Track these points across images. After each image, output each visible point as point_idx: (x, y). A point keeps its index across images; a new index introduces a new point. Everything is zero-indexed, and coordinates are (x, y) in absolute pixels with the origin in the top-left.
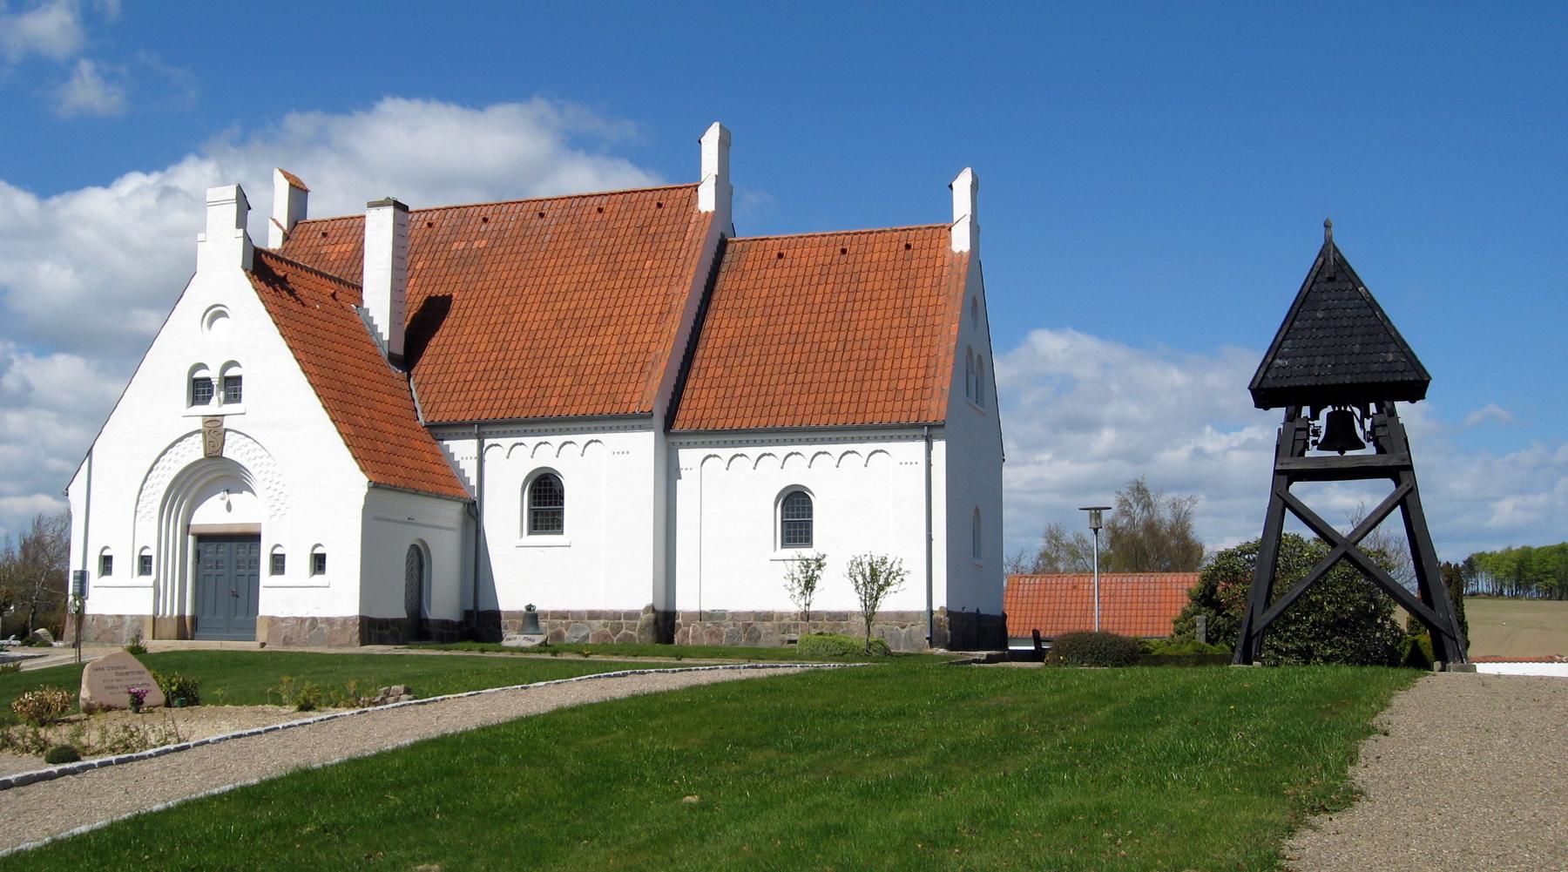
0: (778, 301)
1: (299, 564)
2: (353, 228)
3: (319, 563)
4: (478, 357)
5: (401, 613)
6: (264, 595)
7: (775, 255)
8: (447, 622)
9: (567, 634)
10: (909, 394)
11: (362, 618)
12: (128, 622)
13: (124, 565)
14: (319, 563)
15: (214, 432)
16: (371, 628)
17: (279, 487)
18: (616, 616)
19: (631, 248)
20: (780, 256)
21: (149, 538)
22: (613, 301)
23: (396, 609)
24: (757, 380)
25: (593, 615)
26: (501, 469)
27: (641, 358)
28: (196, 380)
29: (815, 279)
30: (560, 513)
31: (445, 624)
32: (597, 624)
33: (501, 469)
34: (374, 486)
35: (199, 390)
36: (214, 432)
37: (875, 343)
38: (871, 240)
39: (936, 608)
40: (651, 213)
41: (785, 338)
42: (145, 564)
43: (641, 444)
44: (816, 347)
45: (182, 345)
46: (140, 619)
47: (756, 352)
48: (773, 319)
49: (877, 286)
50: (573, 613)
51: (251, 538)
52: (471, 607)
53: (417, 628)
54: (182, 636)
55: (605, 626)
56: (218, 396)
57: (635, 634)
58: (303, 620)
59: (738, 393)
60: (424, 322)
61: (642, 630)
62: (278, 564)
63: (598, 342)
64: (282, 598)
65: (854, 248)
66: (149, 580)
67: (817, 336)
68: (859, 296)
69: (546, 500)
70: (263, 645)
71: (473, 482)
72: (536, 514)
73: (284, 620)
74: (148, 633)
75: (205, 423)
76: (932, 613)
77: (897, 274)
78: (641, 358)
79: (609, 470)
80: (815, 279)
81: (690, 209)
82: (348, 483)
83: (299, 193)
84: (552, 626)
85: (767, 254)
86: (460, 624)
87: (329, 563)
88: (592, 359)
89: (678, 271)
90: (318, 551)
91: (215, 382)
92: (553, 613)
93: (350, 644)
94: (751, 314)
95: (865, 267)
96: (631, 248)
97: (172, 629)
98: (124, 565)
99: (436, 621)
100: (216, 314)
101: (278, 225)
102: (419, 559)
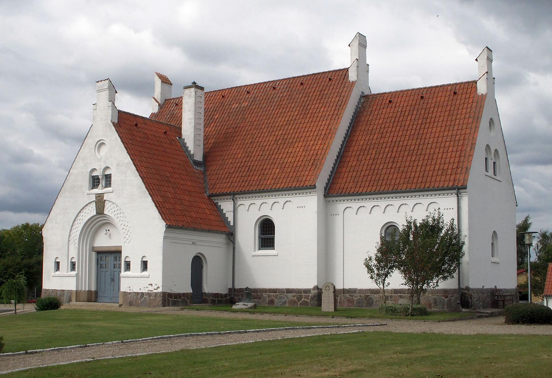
0: (387, 125)
1: (136, 265)
3: (145, 265)
4: (237, 161)
5: (188, 289)
6: (122, 281)
7: (388, 102)
9: (276, 301)
10: (449, 172)
12: (58, 292)
13: (65, 265)
14: (145, 265)
15: (100, 202)
17: (128, 228)
18: (299, 291)
19: (315, 102)
20: (390, 102)
21: (74, 253)
22: (303, 130)
23: (185, 287)
24: (373, 167)
25: (289, 291)
26: (246, 214)
27: (313, 158)
28: (93, 177)
29: (407, 113)
30: (273, 239)
32: (289, 295)
33: (246, 214)
34: (168, 227)
35: (95, 182)
36: (100, 202)
37: (434, 145)
38: (437, 91)
40: (326, 83)
41: (389, 145)
42: (73, 266)
44: (404, 148)
46: (70, 292)
47: (374, 152)
48: (384, 135)
49: (438, 115)
51: (117, 253)
52: (231, 287)
53: (197, 297)
54: (89, 301)
55: (294, 296)
56: (103, 182)
57: (309, 301)
59: (362, 174)
60: (216, 145)
61: (312, 298)
62: (128, 266)
63: (294, 151)
64: (132, 282)
65: (428, 96)
66: (74, 273)
67: (405, 142)
68: (428, 121)
69: (267, 232)
71: (232, 224)
72: (262, 239)
74: (74, 299)
75: (96, 197)
77: (448, 108)
78: (313, 158)
79: (297, 214)
80: (407, 113)
82: (156, 224)
84: (269, 296)
85: (384, 101)
86: (226, 295)
88: (290, 159)
89: (336, 112)
90: (144, 259)
91: (100, 177)
93: (158, 306)
94: (373, 132)
95: (433, 105)
96: (315, 102)
97: (85, 297)
98: (65, 265)
99: (195, 297)
100: (100, 144)
101: (157, 101)
102: (198, 263)
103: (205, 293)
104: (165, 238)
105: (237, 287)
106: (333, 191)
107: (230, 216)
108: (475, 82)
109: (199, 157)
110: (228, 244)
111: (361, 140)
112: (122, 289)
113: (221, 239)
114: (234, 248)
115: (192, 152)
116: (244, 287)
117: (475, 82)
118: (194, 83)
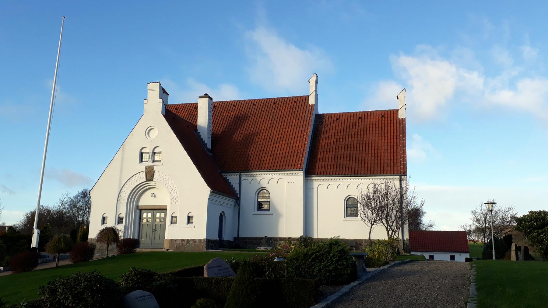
1: (182, 220)
2: (195, 107)
8: (229, 241)
11: (207, 239)
14: (189, 219)
16: (209, 243)
31: (229, 242)
39: (405, 239)
43: (298, 177)
45: (137, 141)
50: (273, 238)
58: (183, 240)
62: (173, 220)
70: (168, 250)
73: (176, 240)
75: (146, 169)
76: (404, 240)
81: (306, 104)
82: (202, 190)
83: (163, 92)
87: (195, 219)
92: (89, 212)
103: (224, 240)
104: (209, 199)
105: (241, 236)
106: (310, 173)
107: (236, 187)
108: (398, 110)
109: (209, 146)
110: (235, 206)
111: (323, 143)
112: (167, 237)
113: (230, 202)
114: (239, 209)
115: (206, 142)
116: (263, 236)
117: (398, 110)
118: (206, 94)
